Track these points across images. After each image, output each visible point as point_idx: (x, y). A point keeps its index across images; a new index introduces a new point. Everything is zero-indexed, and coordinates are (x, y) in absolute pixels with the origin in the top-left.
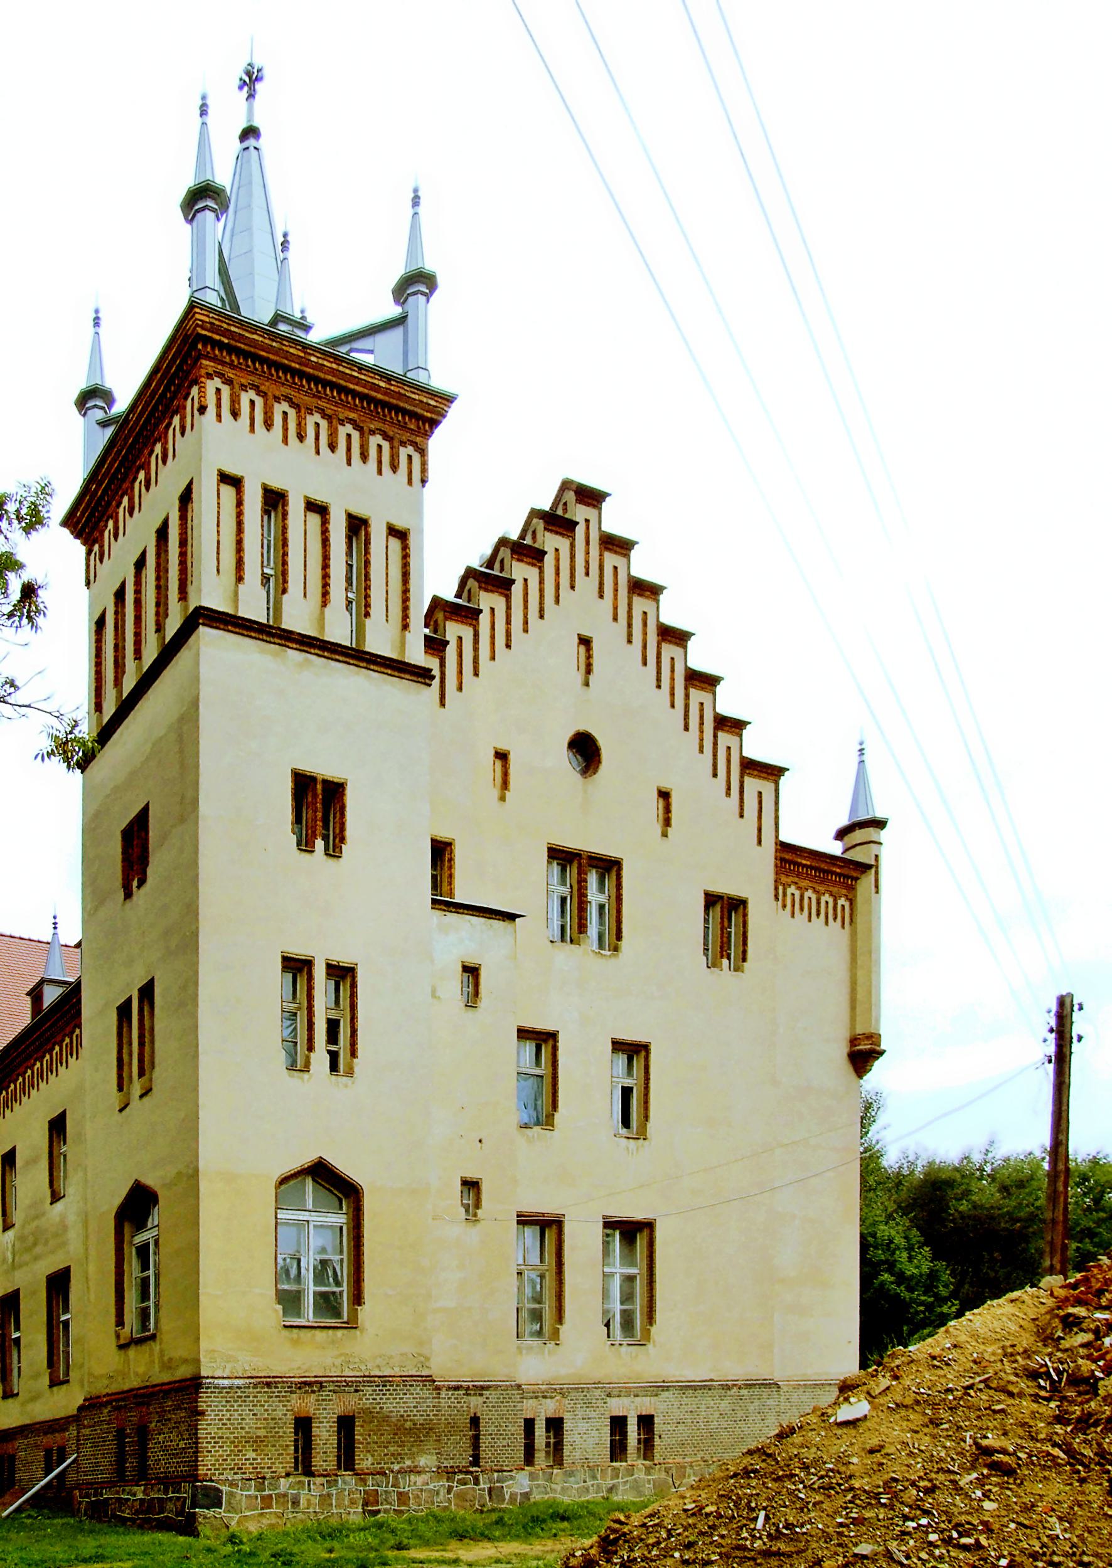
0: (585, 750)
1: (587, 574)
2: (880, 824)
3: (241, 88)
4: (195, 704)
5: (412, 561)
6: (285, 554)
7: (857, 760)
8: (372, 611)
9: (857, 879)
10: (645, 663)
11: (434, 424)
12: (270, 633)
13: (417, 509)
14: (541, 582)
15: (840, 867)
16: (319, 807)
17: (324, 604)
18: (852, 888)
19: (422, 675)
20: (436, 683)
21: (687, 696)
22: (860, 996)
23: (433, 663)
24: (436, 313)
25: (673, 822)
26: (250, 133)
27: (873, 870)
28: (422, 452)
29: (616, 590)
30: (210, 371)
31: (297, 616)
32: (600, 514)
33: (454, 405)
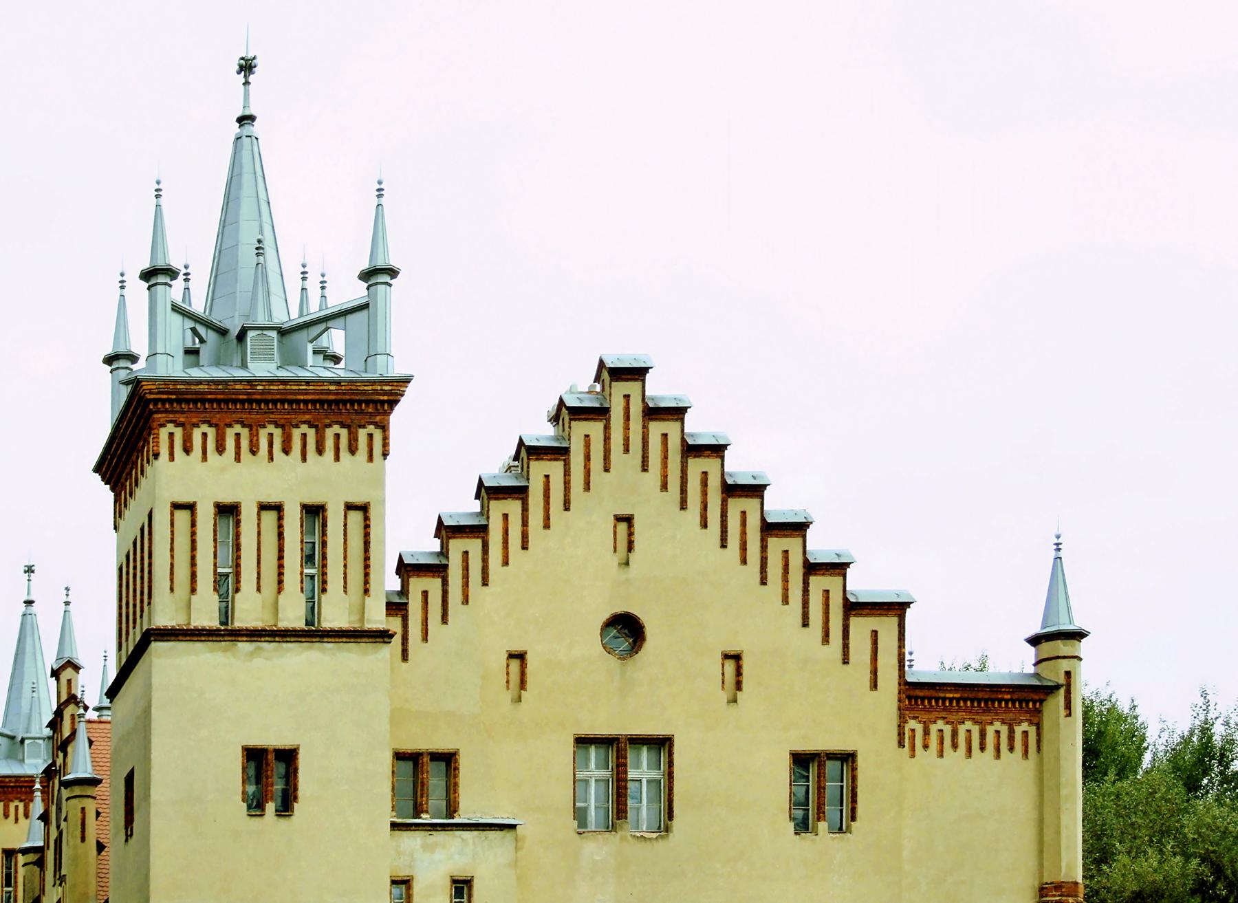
0: (627, 629)
1: (627, 450)
2: (1079, 635)
3: (239, 73)
4: (149, 706)
5: (373, 531)
6: (239, 557)
7: (1053, 554)
8: (329, 587)
9: (1041, 701)
10: (704, 525)
11: (393, 403)
12: (226, 633)
13: (379, 482)
14: (607, 439)
15: (1008, 693)
16: (271, 775)
17: (280, 590)
18: (1039, 712)
19: (383, 636)
20: (397, 640)
21: (764, 548)
22: (1047, 838)
23: (395, 624)
24: (396, 298)
25: (744, 685)
26: (245, 120)
27: (1062, 691)
28: (384, 428)
29: (665, 458)
30: (162, 421)
31: (250, 610)
32: (644, 387)
33: (410, 385)
